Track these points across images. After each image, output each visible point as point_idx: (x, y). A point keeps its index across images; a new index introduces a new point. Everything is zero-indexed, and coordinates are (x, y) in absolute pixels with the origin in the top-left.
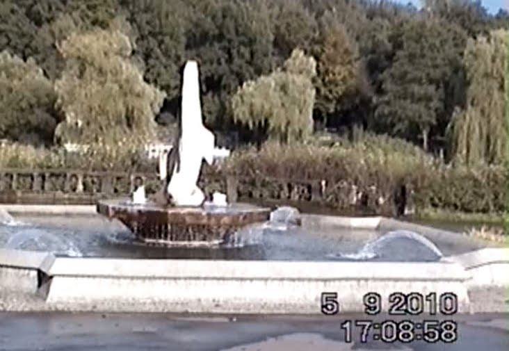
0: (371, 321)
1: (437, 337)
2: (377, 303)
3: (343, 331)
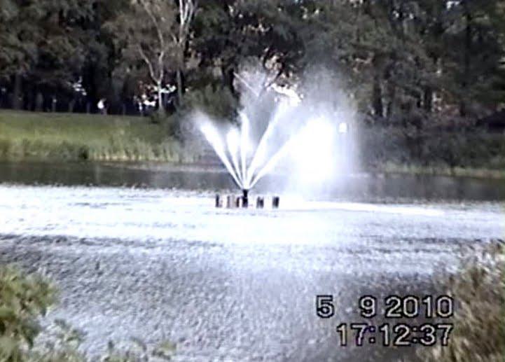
0: (366, 324)
2: (373, 306)
3: (381, 334)
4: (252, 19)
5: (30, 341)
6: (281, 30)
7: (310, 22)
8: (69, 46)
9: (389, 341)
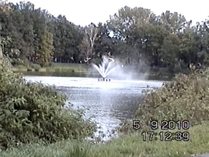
0: (154, 132)
1: (184, 134)
2: (188, 136)
3: (160, 136)
4: (105, 45)
5: (63, 106)
6: (111, 47)
7: (116, 46)
8: (70, 50)
9: (163, 139)
